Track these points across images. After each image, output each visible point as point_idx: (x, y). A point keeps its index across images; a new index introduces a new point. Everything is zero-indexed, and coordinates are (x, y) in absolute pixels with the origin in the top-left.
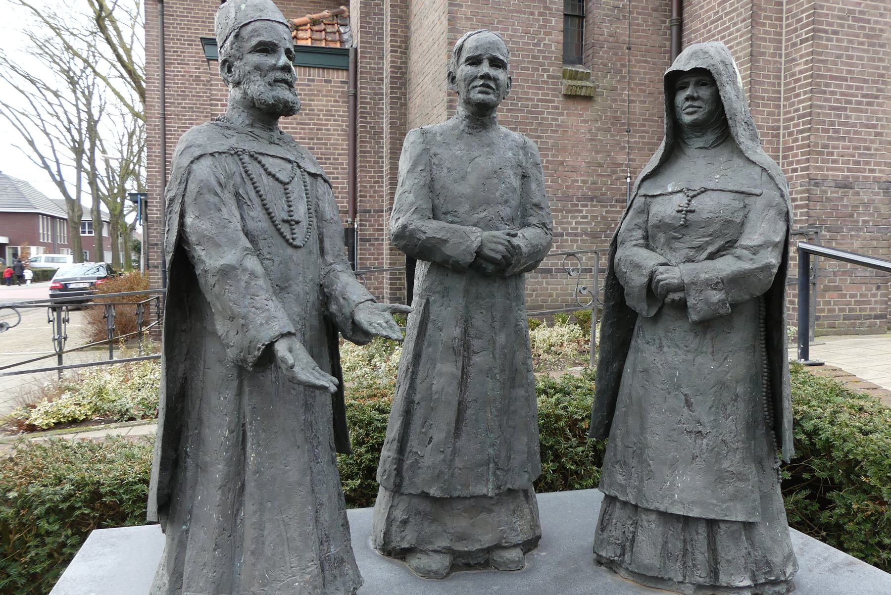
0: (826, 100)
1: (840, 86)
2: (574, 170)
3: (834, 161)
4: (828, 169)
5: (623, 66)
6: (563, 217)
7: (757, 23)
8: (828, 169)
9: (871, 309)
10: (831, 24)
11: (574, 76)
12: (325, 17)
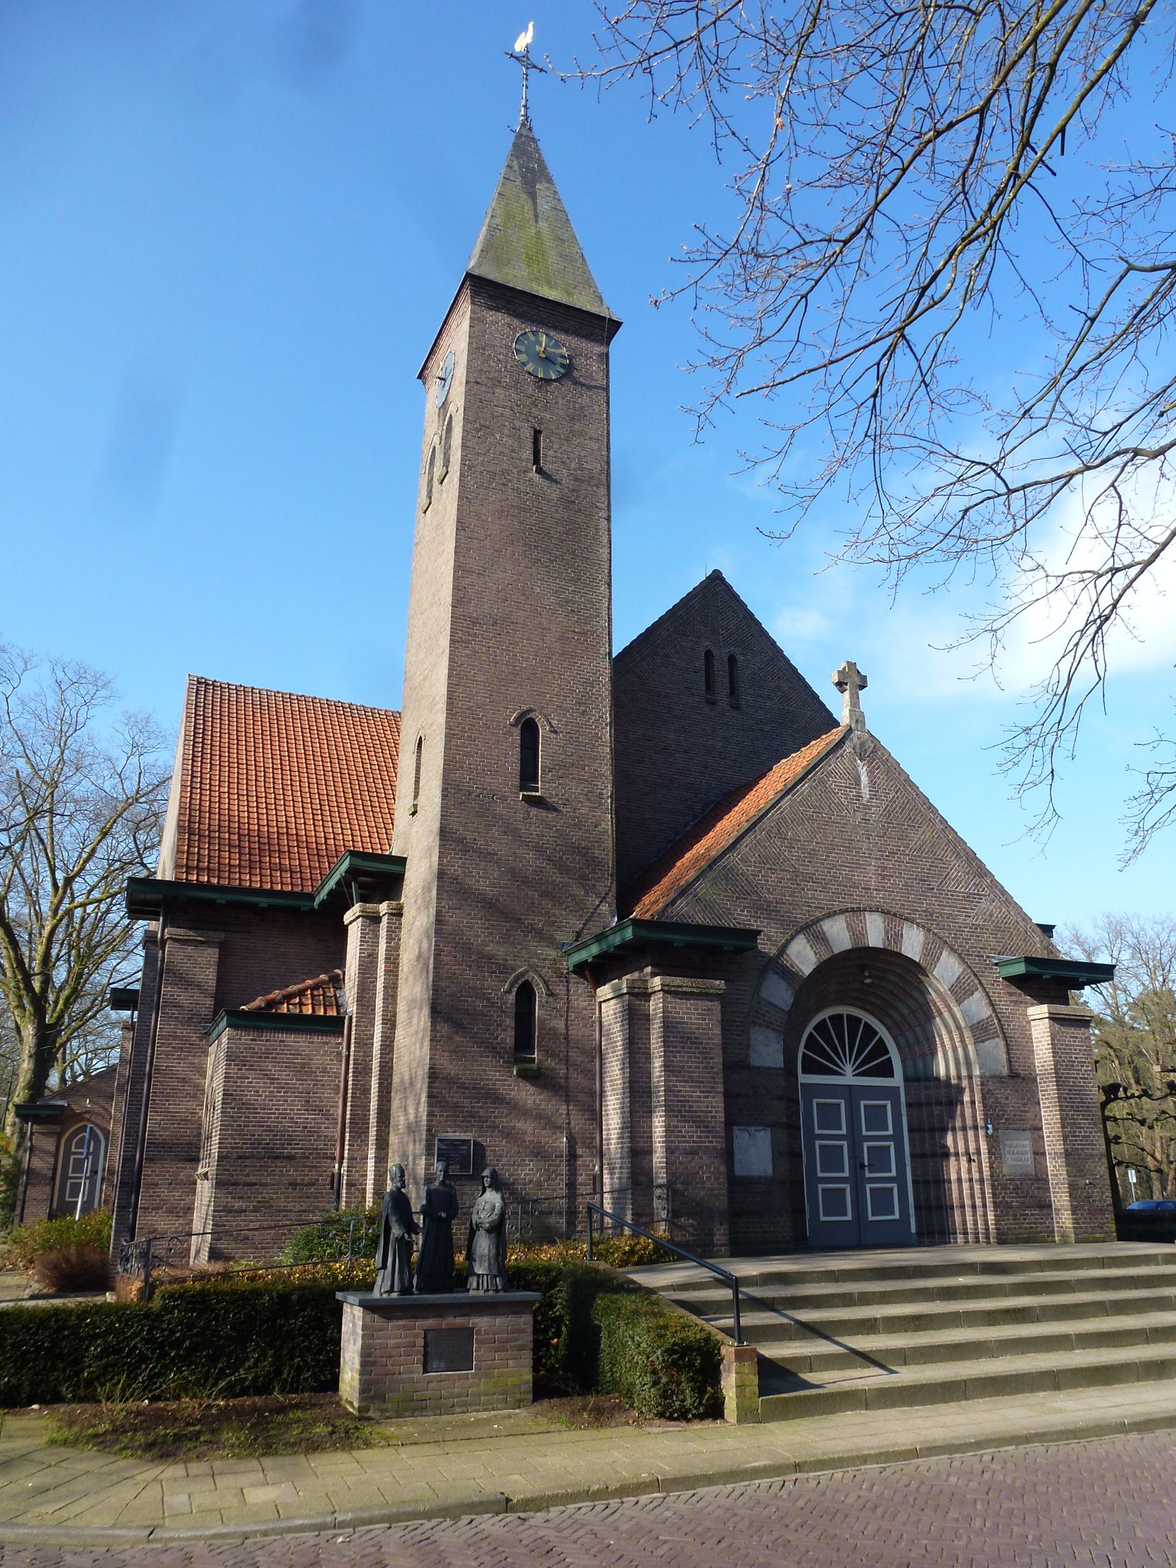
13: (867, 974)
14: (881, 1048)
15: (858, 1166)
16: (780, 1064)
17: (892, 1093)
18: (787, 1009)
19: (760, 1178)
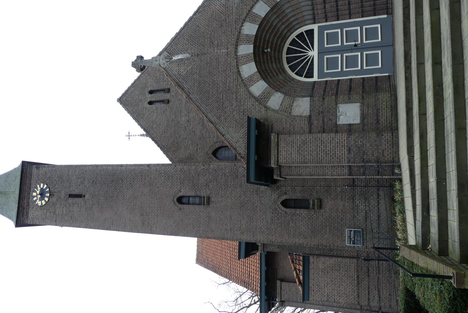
0: (324, 159)
1: (319, 153)
2: (344, 206)
3: (342, 155)
4: (345, 157)
8: (345, 157)
9: (390, 137)
11: (314, 205)
12: (291, 258)
13: (266, 51)
14: (300, 36)
17: (321, 30)
19: (361, 110)
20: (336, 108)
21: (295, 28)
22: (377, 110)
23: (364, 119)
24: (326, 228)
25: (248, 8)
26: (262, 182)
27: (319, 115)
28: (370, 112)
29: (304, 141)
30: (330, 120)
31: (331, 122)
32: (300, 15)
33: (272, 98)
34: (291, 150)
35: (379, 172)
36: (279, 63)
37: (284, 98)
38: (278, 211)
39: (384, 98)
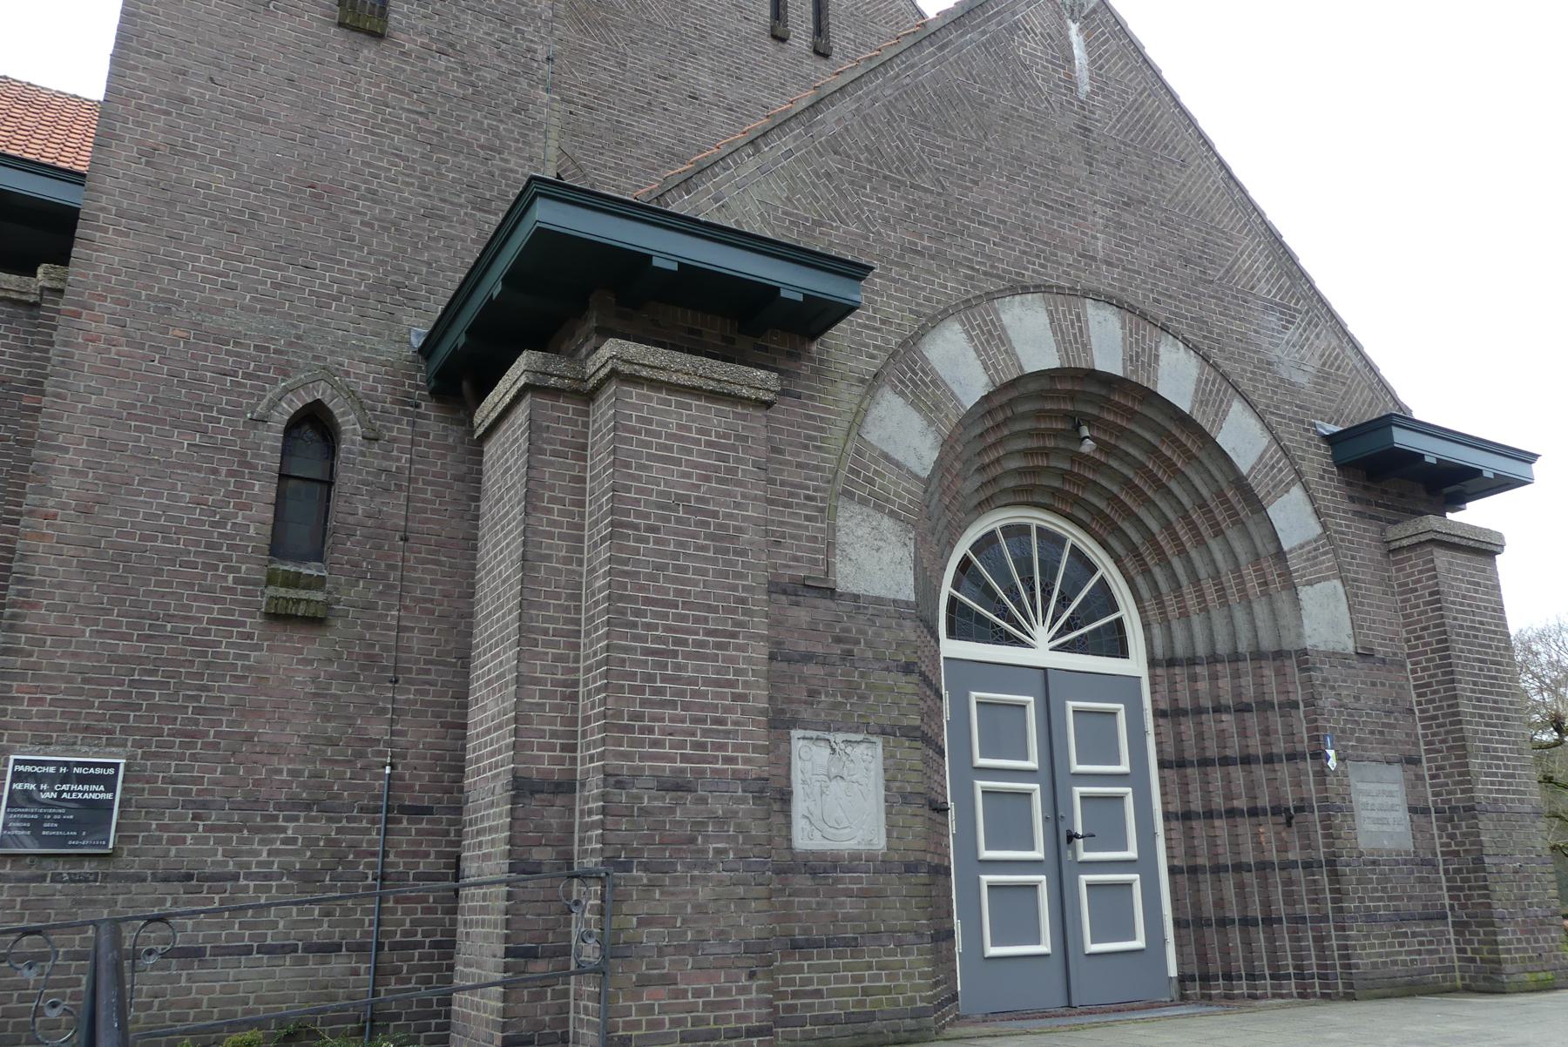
0: (636, 638)
1: (665, 616)
2: (276, 750)
3: (655, 743)
4: (642, 757)
5: (392, 567)
6: (241, 841)
7: (535, 508)
8: (642, 757)
9: (740, 1018)
10: (647, 516)
11: (294, 581)
13: (1085, 431)
14: (1104, 600)
15: (1062, 839)
16: (908, 594)
17: (1125, 687)
18: (925, 474)
19: (855, 856)
20: (863, 727)
21: (1139, 580)
22: (852, 943)
23: (814, 872)
24: (141, 638)
25: (1245, 385)
26: (493, 285)
27: (838, 640)
28: (842, 905)
29: (733, 539)
30: (813, 693)
31: (804, 696)
32: (1191, 602)
33: (916, 421)
34: (690, 464)
35: (530, 954)
36: (1016, 490)
37: (916, 477)
38: (274, 382)
39: (908, 976)
